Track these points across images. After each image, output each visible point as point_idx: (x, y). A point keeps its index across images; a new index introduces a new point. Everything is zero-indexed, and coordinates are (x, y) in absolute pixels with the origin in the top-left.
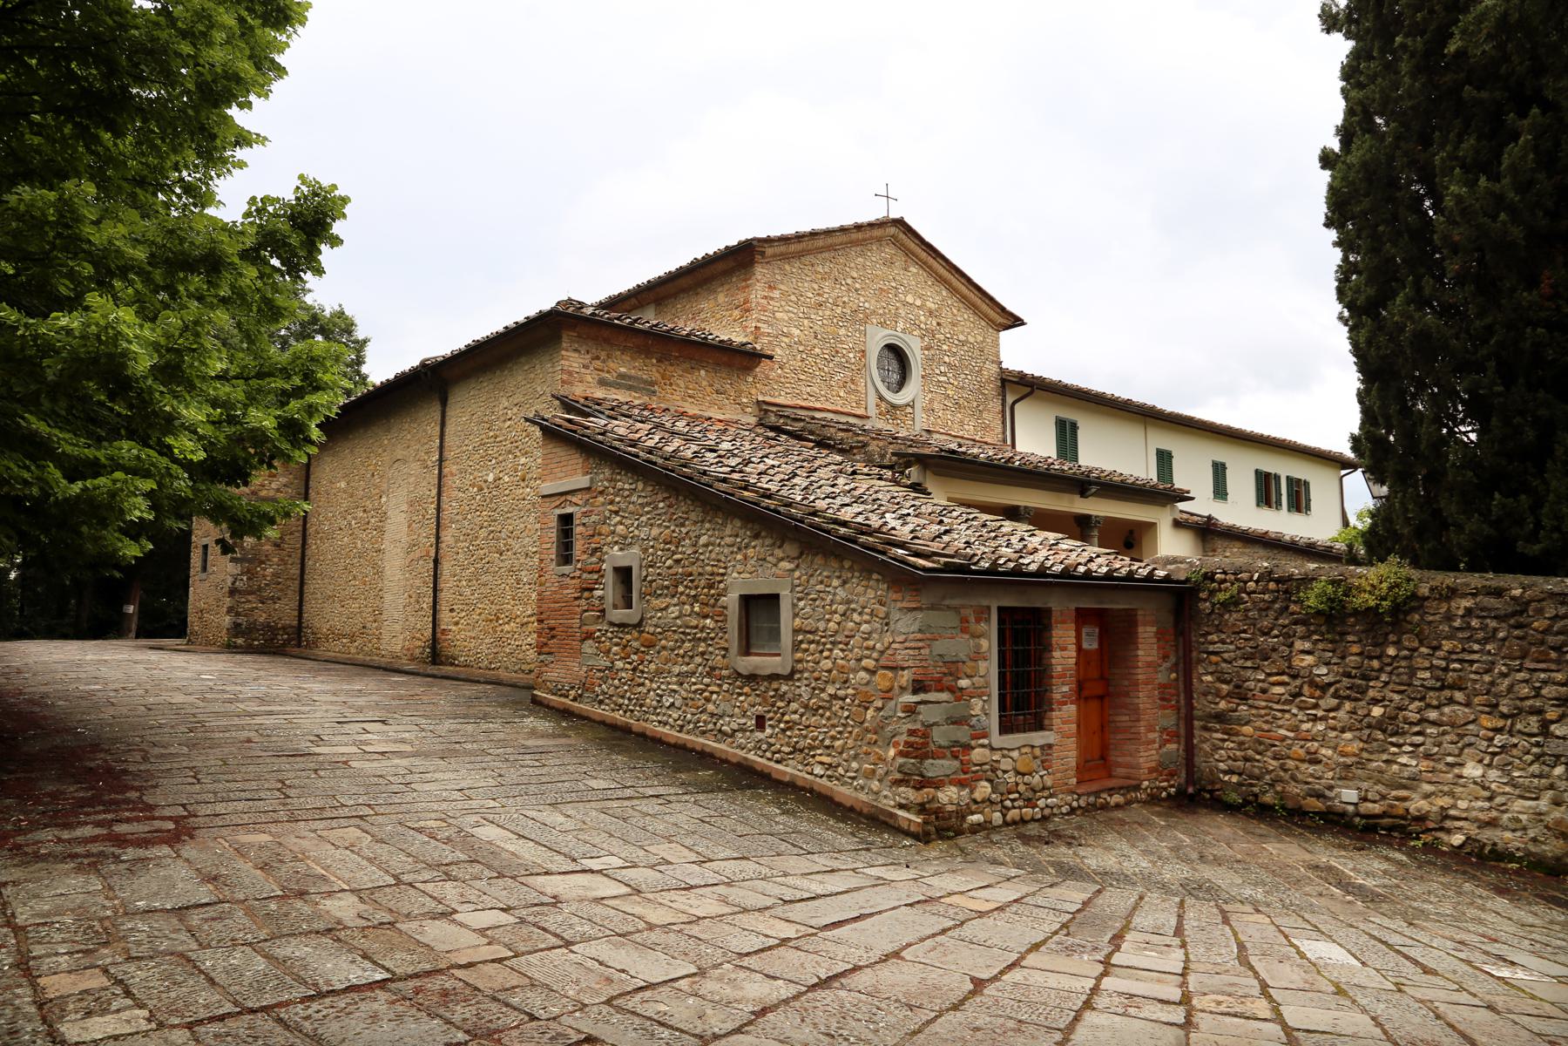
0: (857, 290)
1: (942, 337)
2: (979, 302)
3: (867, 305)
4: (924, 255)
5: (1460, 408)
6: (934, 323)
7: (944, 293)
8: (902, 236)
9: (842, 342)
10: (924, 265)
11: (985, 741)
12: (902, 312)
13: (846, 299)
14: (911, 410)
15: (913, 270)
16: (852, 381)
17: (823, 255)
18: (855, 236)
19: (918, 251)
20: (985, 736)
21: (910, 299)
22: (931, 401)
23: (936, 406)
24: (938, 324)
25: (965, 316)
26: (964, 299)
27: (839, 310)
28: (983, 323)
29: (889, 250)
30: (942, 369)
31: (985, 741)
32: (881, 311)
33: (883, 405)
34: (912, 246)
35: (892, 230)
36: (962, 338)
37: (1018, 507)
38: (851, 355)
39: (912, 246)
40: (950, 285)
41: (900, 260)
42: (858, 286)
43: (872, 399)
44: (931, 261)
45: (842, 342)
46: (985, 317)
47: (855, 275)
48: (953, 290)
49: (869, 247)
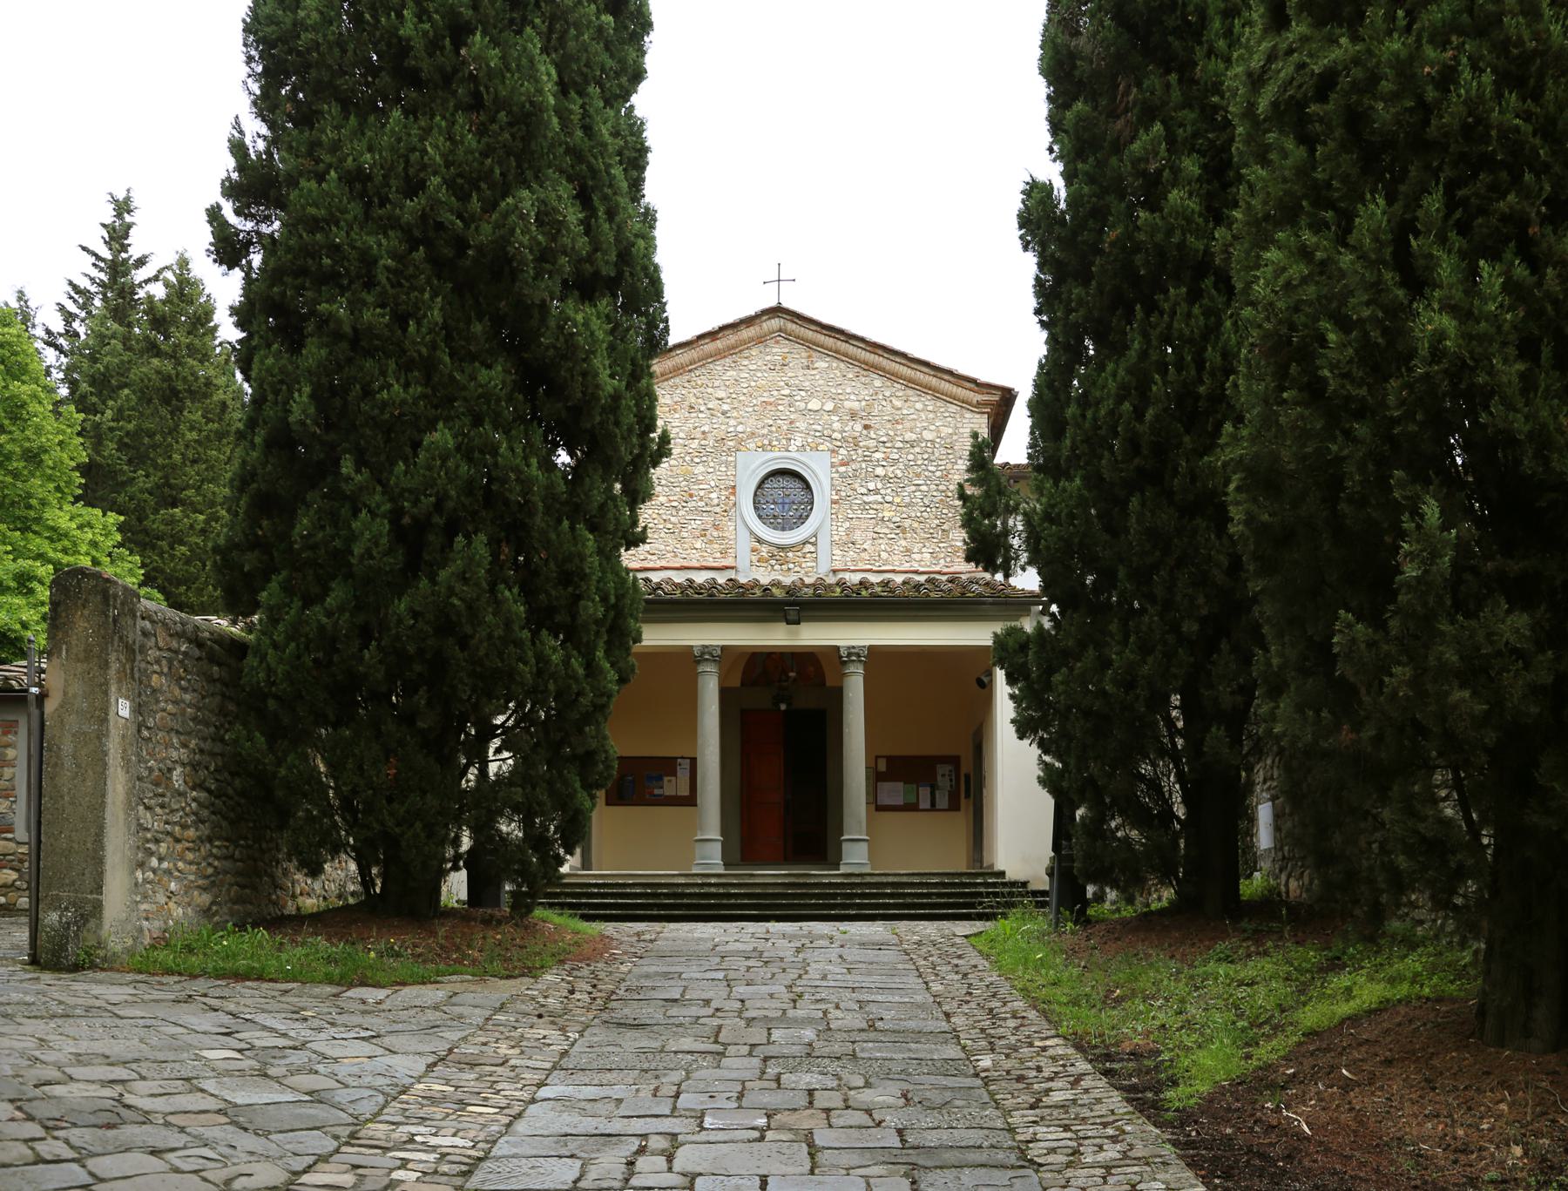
0: (724, 413)
1: (872, 443)
2: (934, 381)
3: (740, 428)
4: (829, 341)
5: (1419, 417)
6: (858, 427)
7: (878, 383)
8: (791, 326)
9: (698, 482)
10: (837, 354)
11: (10, 836)
12: (802, 425)
13: (706, 428)
14: (813, 549)
15: (821, 364)
16: (716, 527)
17: (671, 382)
18: (709, 347)
19: (821, 338)
20: (11, 831)
21: (814, 404)
22: (849, 531)
23: (858, 536)
24: (866, 427)
25: (922, 404)
26: (911, 383)
27: (695, 444)
28: (953, 408)
29: (778, 350)
30: (871, 486)
31: (10, 836)
32: (765, 431)
33: (764, 550)
34: (810, 334)
35: (775, 323)
36: (909, 436)
37: (837, 648)
38: (714, 495)
39: (810, 334)
40: (883, 370)
41: (799, 355)
42: (726, 407)
43: (744, 544)
44: (843, 346)
45: (698, 482)
46: (952, 399)
47: (721, 394)
48: (893, 376)
49: (746, 353)
